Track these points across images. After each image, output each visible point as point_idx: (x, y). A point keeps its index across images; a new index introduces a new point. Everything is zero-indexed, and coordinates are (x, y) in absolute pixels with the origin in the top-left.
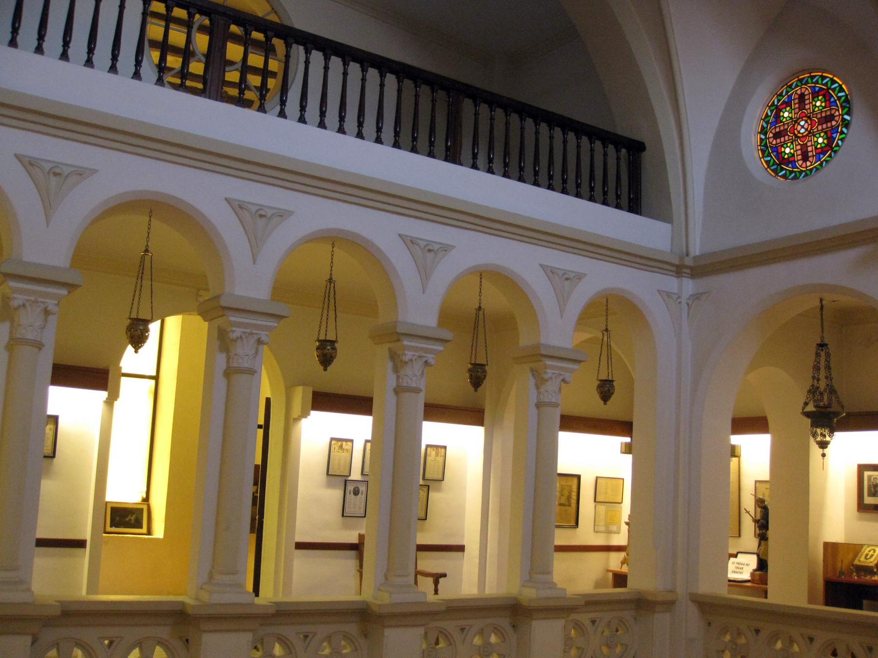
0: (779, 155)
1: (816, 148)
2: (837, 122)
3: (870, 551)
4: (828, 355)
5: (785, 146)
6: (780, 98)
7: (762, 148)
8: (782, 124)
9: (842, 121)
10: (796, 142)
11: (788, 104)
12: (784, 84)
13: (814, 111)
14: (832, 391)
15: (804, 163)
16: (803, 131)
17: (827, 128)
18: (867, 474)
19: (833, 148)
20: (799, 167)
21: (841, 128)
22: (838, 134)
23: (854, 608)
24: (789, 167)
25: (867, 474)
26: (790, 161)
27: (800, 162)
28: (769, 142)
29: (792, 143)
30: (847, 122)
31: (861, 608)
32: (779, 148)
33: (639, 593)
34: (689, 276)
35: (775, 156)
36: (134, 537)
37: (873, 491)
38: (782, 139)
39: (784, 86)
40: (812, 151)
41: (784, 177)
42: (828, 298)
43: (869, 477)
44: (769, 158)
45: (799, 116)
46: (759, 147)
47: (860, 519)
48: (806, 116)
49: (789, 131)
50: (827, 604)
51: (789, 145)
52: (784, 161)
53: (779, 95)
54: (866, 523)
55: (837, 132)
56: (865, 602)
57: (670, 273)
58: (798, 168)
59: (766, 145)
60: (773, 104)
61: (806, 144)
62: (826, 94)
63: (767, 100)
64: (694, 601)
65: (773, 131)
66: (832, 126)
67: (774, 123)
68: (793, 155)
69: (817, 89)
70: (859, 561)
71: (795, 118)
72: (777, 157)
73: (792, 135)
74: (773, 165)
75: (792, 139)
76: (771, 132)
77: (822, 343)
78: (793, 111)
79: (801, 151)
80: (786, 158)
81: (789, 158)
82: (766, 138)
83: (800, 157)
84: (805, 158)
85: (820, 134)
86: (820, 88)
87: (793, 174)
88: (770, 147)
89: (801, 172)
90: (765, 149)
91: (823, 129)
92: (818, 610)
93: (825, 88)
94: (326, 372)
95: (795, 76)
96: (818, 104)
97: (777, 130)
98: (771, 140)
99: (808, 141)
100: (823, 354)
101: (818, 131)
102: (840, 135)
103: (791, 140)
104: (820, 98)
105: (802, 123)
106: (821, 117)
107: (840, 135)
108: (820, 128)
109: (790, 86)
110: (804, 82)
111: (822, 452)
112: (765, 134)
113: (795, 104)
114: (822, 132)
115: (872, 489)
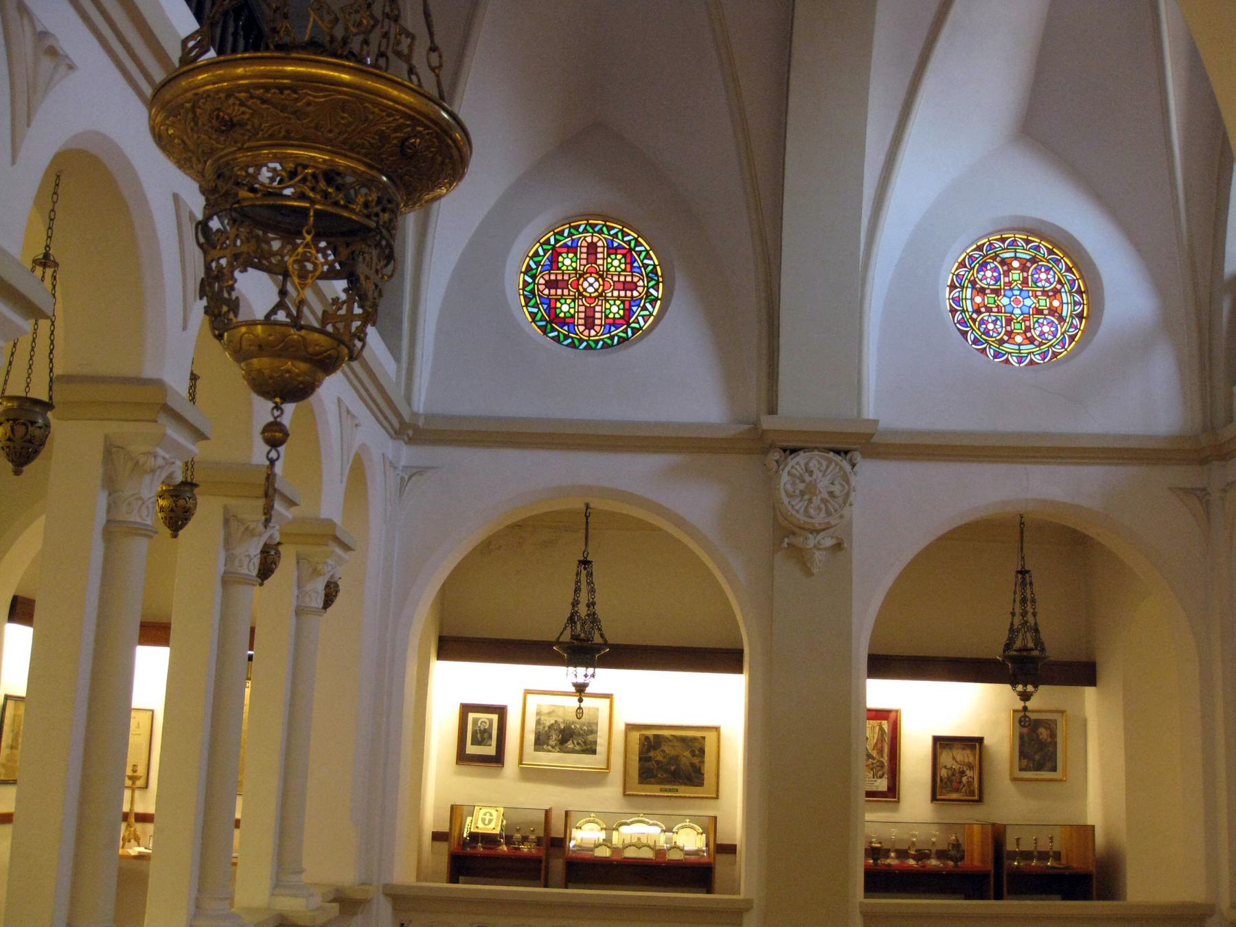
0: (552, 310)
1: (607, 317)
2: (640, 294)
3: (485, 814)
4: (590, 575)
5: (563, 301)
6: (558, 237)
7: (525, 293)
8: (561, 272)
9: (646, 294)
10: (580, 301)
11: (572, 249)
12: (568, 222)
13: (608, 270)
14: (593, 617)
15: (587, 331)
16: (591, 290)
17: (626, 296)
18: (471, 716)
19: (631, 324)
20: (578, 333)
21: (645, 303)
22: (640, 308)
23: (454, 883)
24: (564, 330)
25: (471, 716)
26: (567, 322)
27: (582, 328)
28: (538, 290)
29: (574, 300)
30: (652, 297)
31: (458, 882)
32: (553, 301)
33: (337, 890)
34: (392, 432)
35: (545, 310)
36: (560, 893)
37: (480, 739)
38: (559, 292)
39: (566, 224)
40: (601, 319)
41: (556, 339)
42: (596, 504)
43: (475, 721)
44: (535, 310)
45: (587, 270)
46: (521, 292)
47: (458, 774)
48: (597, 273)
49: (571, 285)
50: (451, 882)
51: (608, 306)
52: (554, 318)
53: (558, 233)
54: (468, 779)
55: (639, 306)
56: (461, 878)
57: (389, 427)
58: (577, 335)
59: (532, 291)
60: (547, 242)
61: (594, 307)
62: (628, 255)
63: (540, 234)
64: (386, 895)
65: (547, 277)
66: (632, 297)
67: (548, 268)
68: (573, 316)
69: (615, 245)
70: (477, 827)
71: (580, 270)
72: (547, 311)
73: (575, 291)
74: (541, 320)
75: (575, 296)
76: (542, 277)
77: (1023, 569)
78: (578, 261)
79: (585, 315)
80: (561, 318)
81: (565, 317)
82: (648, 288)
83: (581, 322)
84: (589, 324)
85: (615, 301)
86: (619, 244)
87: (570, 340)
88: (539, 295)
89: (581, 341)
90: (531, 297)
91: (619, 297)
92: (440, 889)
93: (628, 247)
94: (16, 477)
95: (585, 218)
96: (616, 263)
97: (553, 277)
98: (541, 288)
99: (597, 305)
100: (584, 573)
101: (612, 296)
102: (641, 310)
103: (572, 296)
104: (619, 257)
105: (591, 280)
106: (619, 281)
107: (641, 310)
108: (616, 293)
109: (577, 227)
110: (596, 229)
111: (1023, 705)
112: (534, 277)
113: (581, 253)
114: (618, 300)
115: (479, 736)
